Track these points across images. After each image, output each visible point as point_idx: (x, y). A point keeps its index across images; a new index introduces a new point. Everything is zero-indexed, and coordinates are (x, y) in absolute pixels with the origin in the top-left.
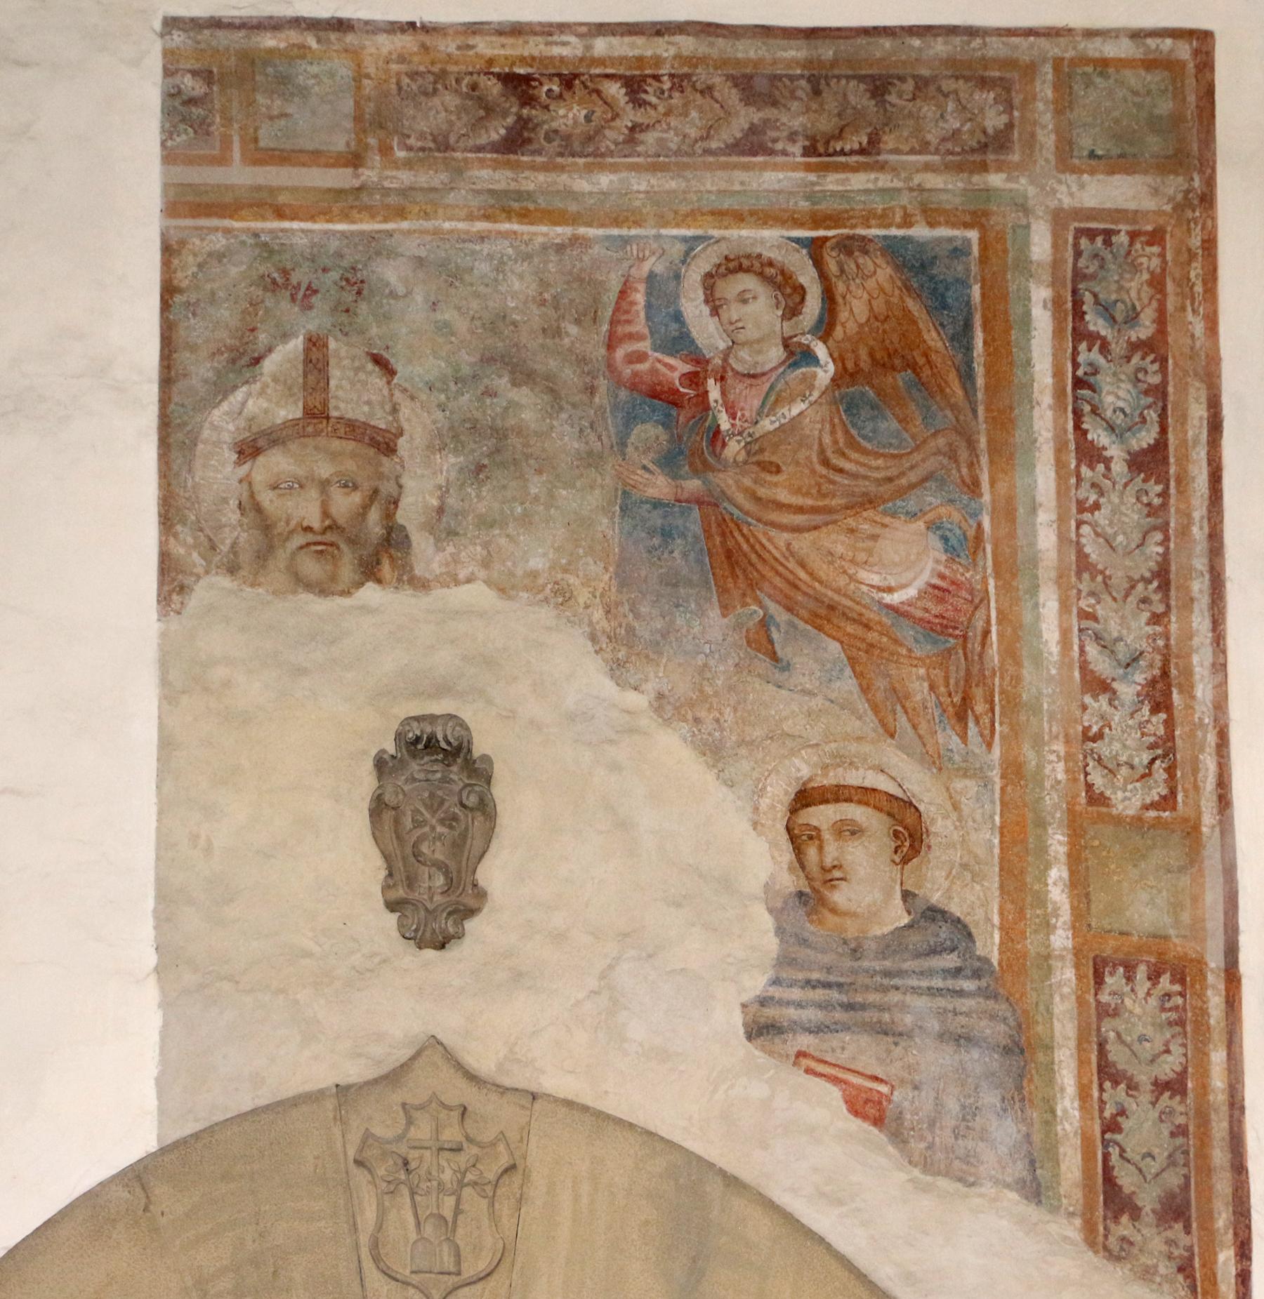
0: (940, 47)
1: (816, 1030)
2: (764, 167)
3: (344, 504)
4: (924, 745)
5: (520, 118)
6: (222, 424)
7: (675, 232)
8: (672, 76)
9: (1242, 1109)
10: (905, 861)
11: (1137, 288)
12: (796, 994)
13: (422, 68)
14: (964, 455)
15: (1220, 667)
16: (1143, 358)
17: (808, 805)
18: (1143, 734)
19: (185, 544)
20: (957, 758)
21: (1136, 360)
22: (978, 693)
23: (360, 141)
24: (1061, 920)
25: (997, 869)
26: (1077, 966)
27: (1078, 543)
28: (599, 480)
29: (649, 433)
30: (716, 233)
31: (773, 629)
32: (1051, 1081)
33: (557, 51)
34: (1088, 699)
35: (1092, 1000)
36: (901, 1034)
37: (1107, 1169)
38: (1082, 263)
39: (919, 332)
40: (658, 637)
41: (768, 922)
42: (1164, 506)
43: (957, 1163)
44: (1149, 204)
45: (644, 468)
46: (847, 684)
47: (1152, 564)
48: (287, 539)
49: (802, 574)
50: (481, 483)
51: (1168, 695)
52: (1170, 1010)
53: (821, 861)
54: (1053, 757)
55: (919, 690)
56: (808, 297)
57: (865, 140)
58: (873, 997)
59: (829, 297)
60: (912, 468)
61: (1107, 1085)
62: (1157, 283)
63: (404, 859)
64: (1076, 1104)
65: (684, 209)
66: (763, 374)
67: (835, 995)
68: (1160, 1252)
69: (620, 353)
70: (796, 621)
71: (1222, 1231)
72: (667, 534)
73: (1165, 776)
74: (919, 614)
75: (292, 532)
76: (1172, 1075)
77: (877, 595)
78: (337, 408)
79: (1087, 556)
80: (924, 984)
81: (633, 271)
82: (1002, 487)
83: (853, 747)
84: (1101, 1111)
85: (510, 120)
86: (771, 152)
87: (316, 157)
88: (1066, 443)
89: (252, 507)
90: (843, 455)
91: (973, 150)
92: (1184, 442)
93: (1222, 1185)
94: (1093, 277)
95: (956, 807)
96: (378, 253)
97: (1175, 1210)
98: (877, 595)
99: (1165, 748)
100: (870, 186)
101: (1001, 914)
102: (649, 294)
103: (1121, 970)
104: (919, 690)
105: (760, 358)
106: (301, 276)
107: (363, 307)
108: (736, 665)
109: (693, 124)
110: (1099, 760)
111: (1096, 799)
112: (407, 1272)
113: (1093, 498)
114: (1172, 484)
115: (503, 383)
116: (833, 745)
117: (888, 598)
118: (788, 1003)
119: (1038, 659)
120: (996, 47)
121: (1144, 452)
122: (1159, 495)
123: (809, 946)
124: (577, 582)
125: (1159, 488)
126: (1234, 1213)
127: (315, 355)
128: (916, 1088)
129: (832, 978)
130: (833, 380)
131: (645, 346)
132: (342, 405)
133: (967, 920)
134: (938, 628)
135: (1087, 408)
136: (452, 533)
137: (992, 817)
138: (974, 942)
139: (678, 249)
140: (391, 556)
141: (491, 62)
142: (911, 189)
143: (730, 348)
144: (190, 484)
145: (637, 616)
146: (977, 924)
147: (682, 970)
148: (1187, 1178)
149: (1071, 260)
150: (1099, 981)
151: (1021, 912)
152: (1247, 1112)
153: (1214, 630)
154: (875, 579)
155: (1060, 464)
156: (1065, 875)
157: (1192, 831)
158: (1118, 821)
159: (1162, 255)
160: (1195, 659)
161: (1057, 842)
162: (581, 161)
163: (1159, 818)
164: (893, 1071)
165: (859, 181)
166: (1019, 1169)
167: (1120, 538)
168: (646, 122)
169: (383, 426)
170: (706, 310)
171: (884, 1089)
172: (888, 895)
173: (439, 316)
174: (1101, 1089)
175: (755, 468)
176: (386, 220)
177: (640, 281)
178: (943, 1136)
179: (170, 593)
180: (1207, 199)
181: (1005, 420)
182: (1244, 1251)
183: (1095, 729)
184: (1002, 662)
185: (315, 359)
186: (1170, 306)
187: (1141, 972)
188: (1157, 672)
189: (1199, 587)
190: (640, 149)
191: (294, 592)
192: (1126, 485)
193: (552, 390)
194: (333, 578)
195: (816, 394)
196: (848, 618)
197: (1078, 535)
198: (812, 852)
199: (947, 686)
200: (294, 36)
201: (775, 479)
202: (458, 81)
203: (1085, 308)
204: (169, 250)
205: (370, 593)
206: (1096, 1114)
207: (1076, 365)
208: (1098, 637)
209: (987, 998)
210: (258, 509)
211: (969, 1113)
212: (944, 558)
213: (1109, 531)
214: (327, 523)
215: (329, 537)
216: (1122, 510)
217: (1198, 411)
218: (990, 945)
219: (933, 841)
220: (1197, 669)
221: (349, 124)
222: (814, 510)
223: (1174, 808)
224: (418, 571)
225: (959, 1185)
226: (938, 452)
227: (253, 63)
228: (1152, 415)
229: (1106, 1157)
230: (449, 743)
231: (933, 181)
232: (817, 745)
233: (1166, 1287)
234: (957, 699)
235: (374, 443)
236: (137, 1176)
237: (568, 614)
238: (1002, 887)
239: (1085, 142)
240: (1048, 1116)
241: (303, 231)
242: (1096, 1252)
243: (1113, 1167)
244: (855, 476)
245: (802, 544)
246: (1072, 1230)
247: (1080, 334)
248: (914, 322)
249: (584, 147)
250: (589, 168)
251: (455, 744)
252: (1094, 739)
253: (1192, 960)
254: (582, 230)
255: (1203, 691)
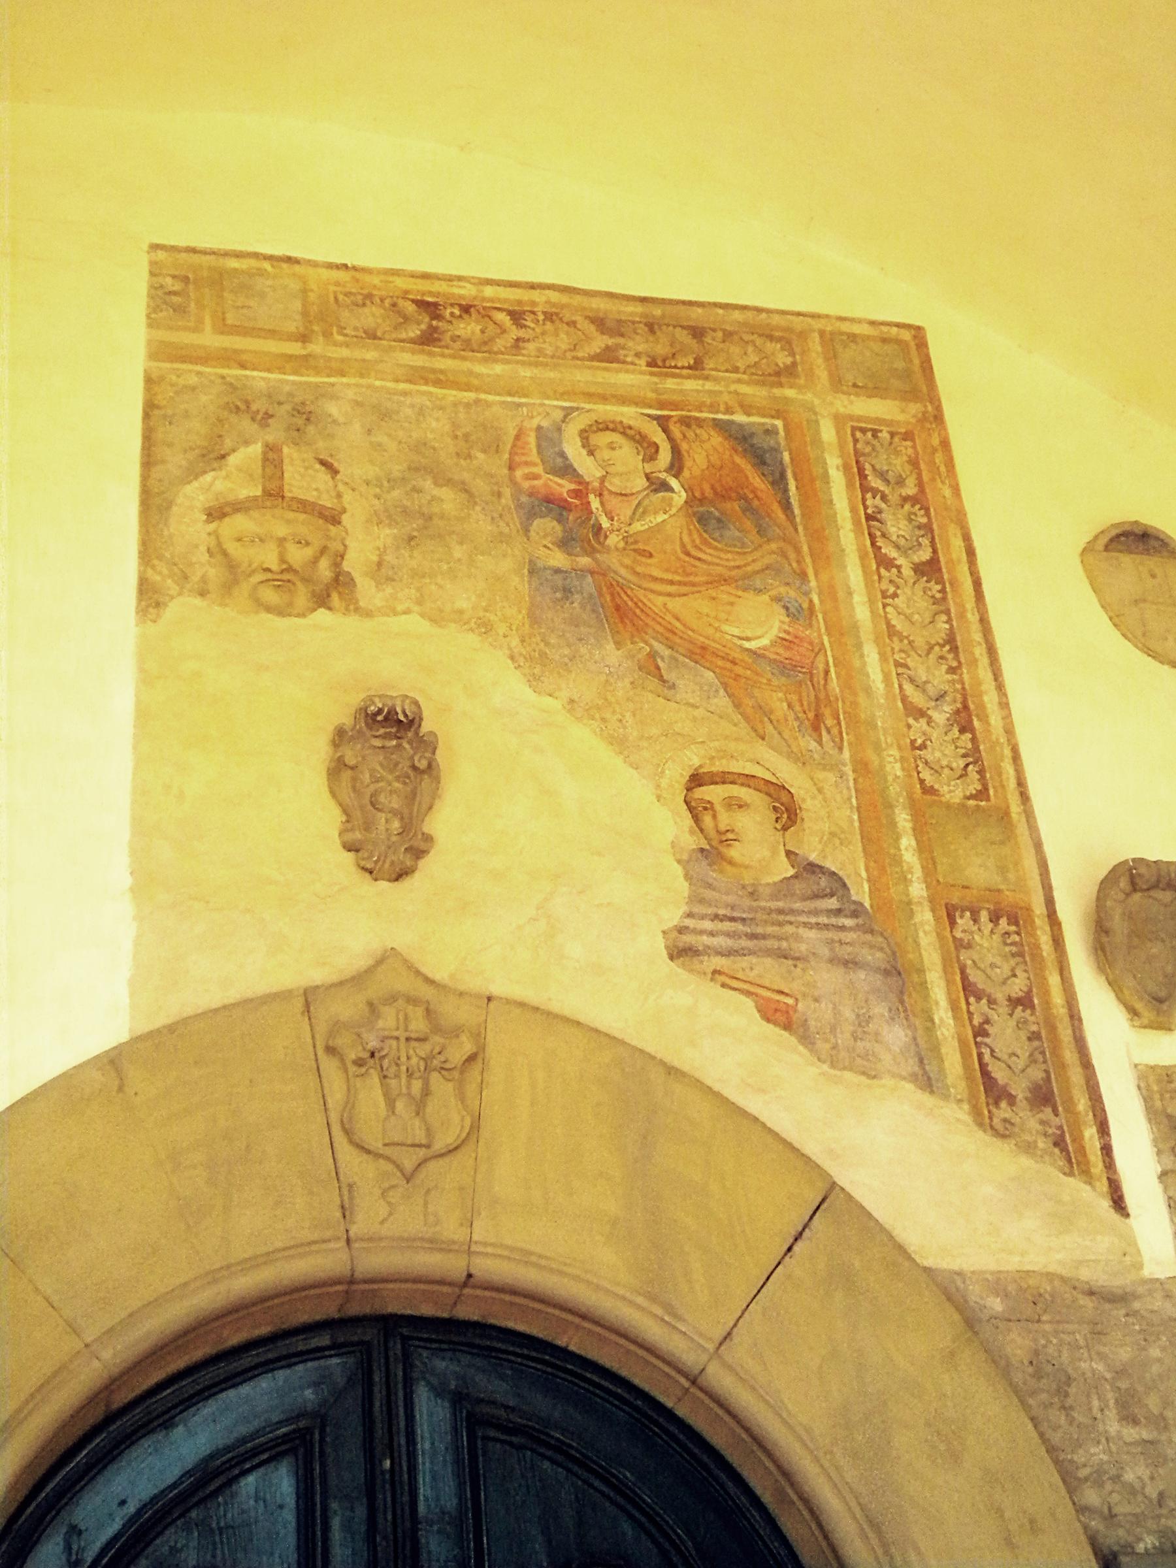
0: (737, 315)
1: (729, 953)
2: (618, 371)
3: (298, 556)
4: (789, 746)
5: (430, 326)
6: (195, 496)
7: (555, 403)
8: (544, 313)
9: (1080, 1020)
10: (785, 828)
11: (899, 465)
12: (708, 925)
13: (353, 290)
14: (792, 556)
15: (1004, 705)
16: (913, 506)
17: (700, 785)
18: (957, 747)
19: (160, 573)
20: (816, 756)
21: (907, 507)
22: (827, 712)
23: (306, 328)
24: (916, 876)
25: (859, 837)
26: (933, 910)
27: (886, 617)
28: (510, 551)
29: (546, 526)
30: (587, 406)
31: (659, 660)
32: (926, 997)
33: (456, 291)
34: (911, 721)
35: (949, 935)
36: (798, 959)
37: (983, 1066)
38: (859, 446)
39: (747, 478)
40: (566, 660)
41: (679, 870)
42: (944, 599)
43: (859, 1061)
44: (901, 417)
45: (545, 546)
46: (722, 701)
47: (944, 635)
48: (249, 576)
49: (678, 625)
50: (412, 549)
51: (971, 721)
52: (1011, 944)
53: (716, 826)
54: (891, 759)
55: (779, 706)
56: (661, 450)
57: (692, 362)
58: (770, 929)
59: (676, 451)
60: (754, 561)
61: (972, 1000)
62: (914, 463)
63: (362, 807)
64: (950, 1014)
65: (561, 390)
66: (633, 494)
67: (740, 927)
68: (1037, 1132)
69: (519, 473)
70: (677, 655)
71: (1083, 1113)
72: (567, 591)
73: (978, 777)
74: (773, 656)
75: (254, 571)
76: (1021, 994)
77: (739, 642)
78: (291, 491)
79: (894, 626)
80: (813, 920)
81: (525, 424)
82: (824, 577)
83: (732, 746)
84: (971, 1020)
85: (423, 327)
86: (624, 362)
87: (272, 334)
88: (866, 553)
89: (219, 551)
90: (700, 549)
91: (770, 375)
92: (950, 561)
93: (1076, 1076)
94: (869, 455)
95: (820, 790)
96: (323, 396)
97: (1042, 1097)
98: (739, 642)
99: (974, 756)
100: (700, 388)
101: (867, 870)
102: (538, 438)
103: (968, 914)
104: (779, 706)
105: (628, 484)
106: (258, 405)
107: (311, 429)
108: (632, 683)
109: (563, 341)
110: (926, 763)
111: (928, 790)
112: (380, 1145)
113: (892, 590)
114: (948, 585)
115: (428, 484)
116: (717, 744)
117: (747, 645)
118: (702, 932)
119: (868, 691)
120: (776, 320)
121: (923, 564)
122: (939, 592)
123: (714, 890)
124: (496, 619)
125: (939, 587)
126: (1090, 1099)
127: (271, 455)
128: (816, 1000)
129: (735, 914)
130: (686, 502)
131: (539, 470)
132: (294, 490)
133: (841, 873)
134: (786, 668)
135: (878, 534)
136: (390, 579)
137: (849, 799)
138: (848, 890)
139: (558, 415)
140: (340, 593)
141: (407, 292)
142: (730, 393)
143: (604, 477)
144: (166, 533)
145: (547, 644)
146: (849, 876)
147: (609, 904)
148: (1047, 1072)
149: (851, 445)
150: (952, 923)
151: (883, 870)
152: (1084, 1022)
153: (996, 680)
154: (736, 632)
155: (865, 567)
156: (914, 843)
157: (1004, 815)
158: (948, 806)
159: (914, 447)
160: (986, 698)
161: (903, 819)
162: (479, 355)
163: (978, 806)
164: (795, 987)
165: (690, 385)
166: (912, 1066)
167: (916, 617)
168: (527, 337)
169: (330, 506)
170: (584, 452)
171: (790, 1001)
172: (774, 852)
173: (373, 439)
174: (968, 1003)
175: (632, 553)
176: (328, 376)
177: (531, 429)
178: (844, 1037)
179: (148, 606)
180: (939, 418)
181: (821, 538)
182: (1103, 1128)
183: (919, 741)
184: (841, 691)
185: (272, 459)
186: (926, 478)
187: (984, 916)
188: (959, 705)
189: (980, 651)
190: (524, 352)
191: (257, 612)
192: (914, 583)
193: (466, 491)
194: (290, 604)
195: (674, 510)
196: (718, 656)
197: (886, 613)
198: (707, 820)
199: (802, 705)
200: (253, 263)
201: (649, 561)
202: (382, 300)
203: (867, 472)
204: (149, 381)
205: (322, 615)
206: (967, 1023)
207: (866, 507)
208: (912, 680)
209: (865, 932)
210: (225, 554)
211: (863, 1021)
212: (787, 620)
213: (908, 612)
214: (284, 566)
215: (286, 576)
216: (914, 600)
217: (957, 543)
218: (861, 893)
219: (805, 814)
220: (989, 706)
221: (298, 317)
222: (680, 583)
223: (988, 800)
224: (361, 604)
225: (863, 1078)
226: (773, 552)
227: (221, 274)
228: (925, 542)
229: (980, 1056)
230: (406, 716)
231: (744, 389)
232: (703, 742)
233: (1047, 1158)
234: (811, 715)
235: (321, 515)
236: (113, 1061)
237: (490, 640)
238: (864, 850)
239: (849, 378)
240: (929, 1024)
241: (262, 378)
242: (985, 1131)
243: (987, 1064)
244: (709, 564)
245: (675, 604)
246: (962, 1113)
247: (865, 489)
248: (741, 471)
249: (483, 348)
250: (485, 360)
251: (411, 716)
252: (920, 748)
253: (1021, 908)
254: (483, 396)
255: (995, 719)
